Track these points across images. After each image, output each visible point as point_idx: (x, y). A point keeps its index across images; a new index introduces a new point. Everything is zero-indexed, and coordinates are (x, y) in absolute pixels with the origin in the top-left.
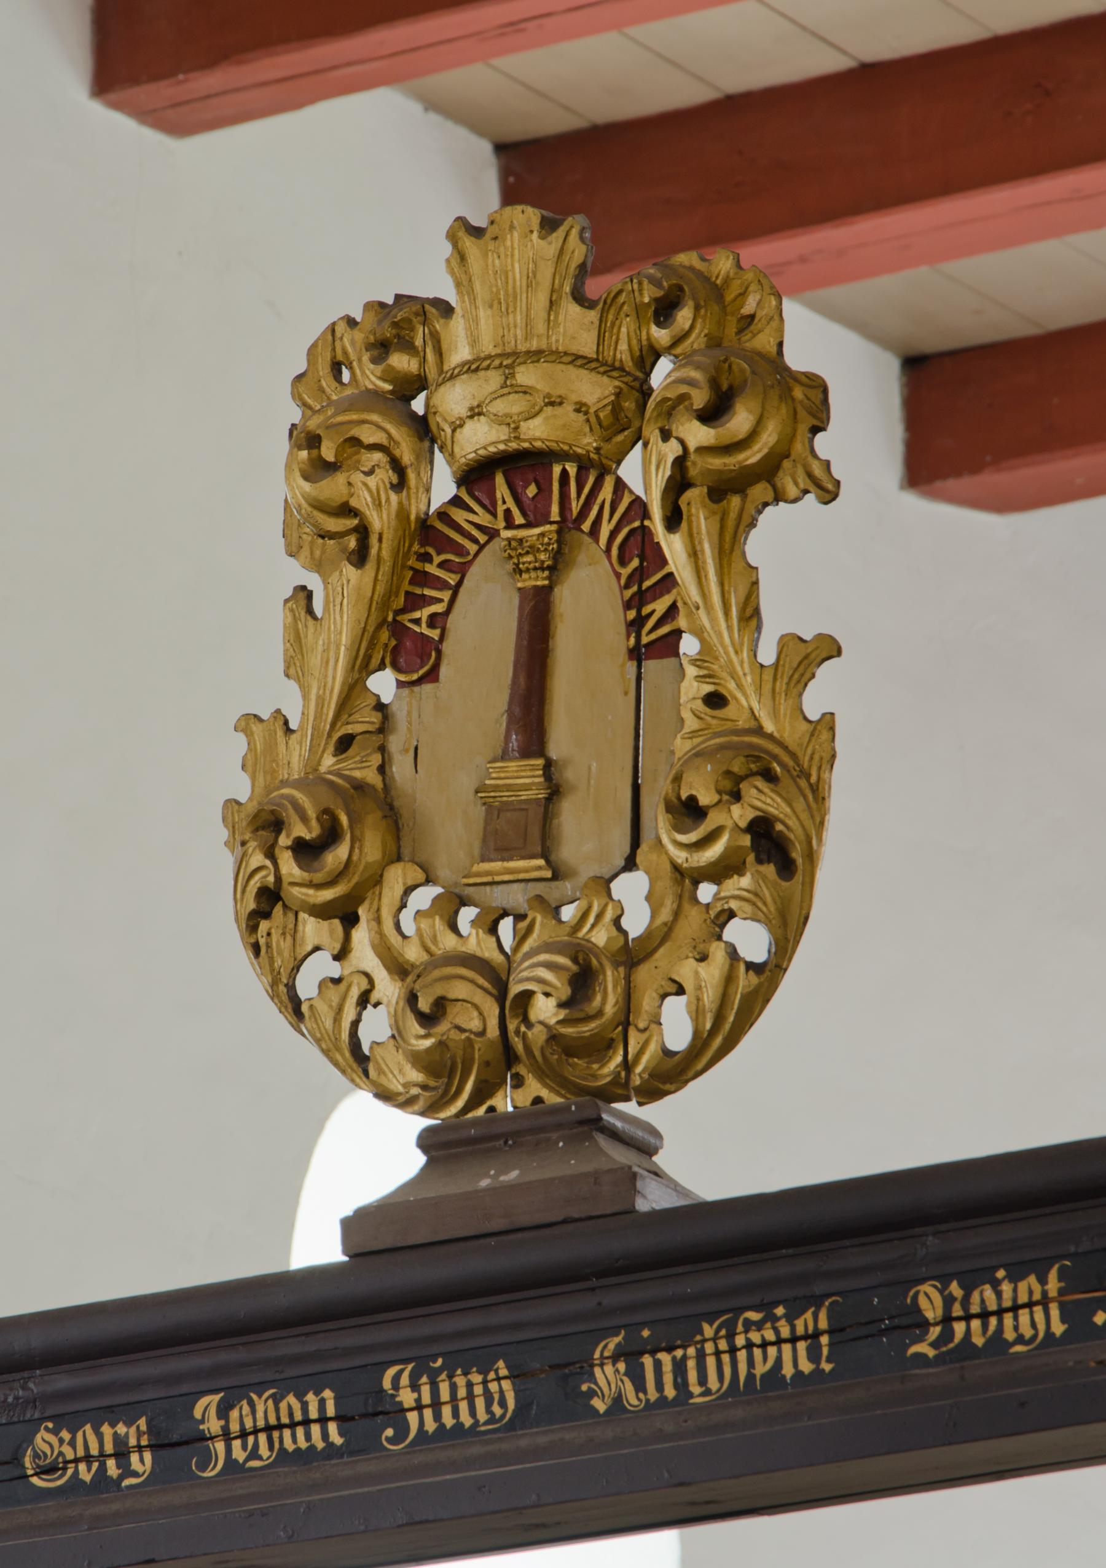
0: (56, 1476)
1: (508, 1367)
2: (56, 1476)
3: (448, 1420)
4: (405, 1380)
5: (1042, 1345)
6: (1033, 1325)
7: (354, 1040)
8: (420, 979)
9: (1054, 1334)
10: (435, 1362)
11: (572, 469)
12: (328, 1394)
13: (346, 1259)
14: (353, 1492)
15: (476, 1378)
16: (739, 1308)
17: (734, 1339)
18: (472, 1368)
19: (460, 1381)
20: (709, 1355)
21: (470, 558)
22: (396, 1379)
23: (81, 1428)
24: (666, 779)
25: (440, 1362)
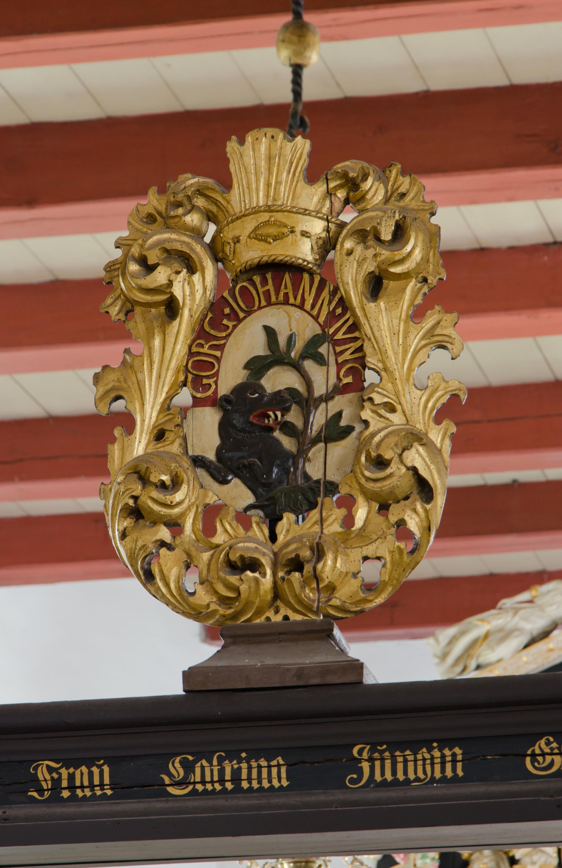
0: (182, 787)
1: (283, 760)
2: (182, 787)
3: (449, 773)
4: (365, 755)
5: (366, 785)
6: (425, 772)
7: (546, 576)
8: (231, 550)
9: (435, 778)
10: (99, 761)
11: (292, 300)
12: (106, 769)
13: (184, 693)
14: (283, 811)
15: (263, 763)
16: (32, 761)
17: (248, 766)
18: (252, 760)
19: (254, 764)
20: (401, 762)
21: (229, 330)
22: (360, 752)
23: (79, 768)
24: (391, 475)
25: (385, 747)
